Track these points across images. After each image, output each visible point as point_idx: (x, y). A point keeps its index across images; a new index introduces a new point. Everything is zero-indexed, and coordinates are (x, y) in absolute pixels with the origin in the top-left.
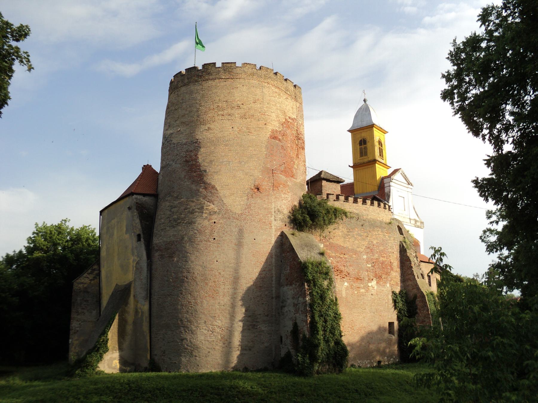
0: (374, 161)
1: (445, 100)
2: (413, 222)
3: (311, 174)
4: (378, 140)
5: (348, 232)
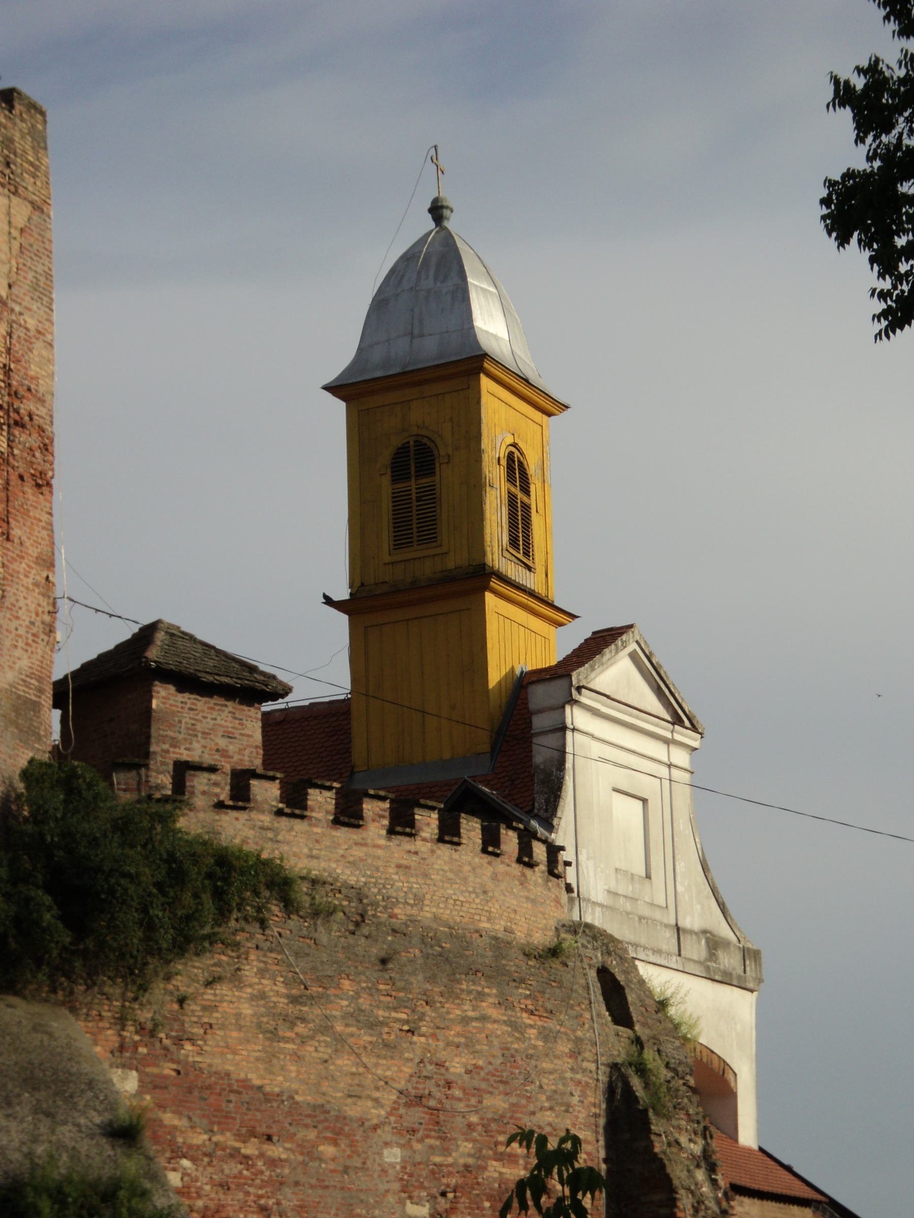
0: (480, 577)
1: (843, 241)
2: (696, 949)
3: (84, 641)
4: (503, 453)
5: (295, 1000)
